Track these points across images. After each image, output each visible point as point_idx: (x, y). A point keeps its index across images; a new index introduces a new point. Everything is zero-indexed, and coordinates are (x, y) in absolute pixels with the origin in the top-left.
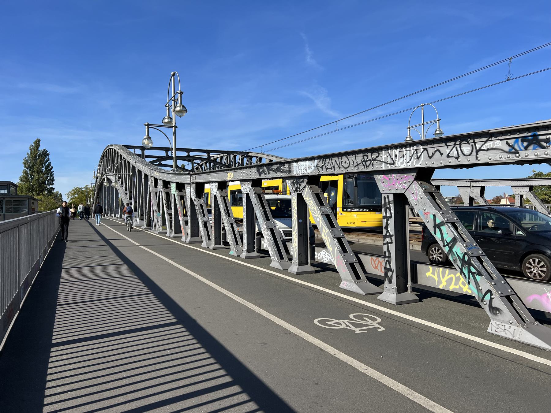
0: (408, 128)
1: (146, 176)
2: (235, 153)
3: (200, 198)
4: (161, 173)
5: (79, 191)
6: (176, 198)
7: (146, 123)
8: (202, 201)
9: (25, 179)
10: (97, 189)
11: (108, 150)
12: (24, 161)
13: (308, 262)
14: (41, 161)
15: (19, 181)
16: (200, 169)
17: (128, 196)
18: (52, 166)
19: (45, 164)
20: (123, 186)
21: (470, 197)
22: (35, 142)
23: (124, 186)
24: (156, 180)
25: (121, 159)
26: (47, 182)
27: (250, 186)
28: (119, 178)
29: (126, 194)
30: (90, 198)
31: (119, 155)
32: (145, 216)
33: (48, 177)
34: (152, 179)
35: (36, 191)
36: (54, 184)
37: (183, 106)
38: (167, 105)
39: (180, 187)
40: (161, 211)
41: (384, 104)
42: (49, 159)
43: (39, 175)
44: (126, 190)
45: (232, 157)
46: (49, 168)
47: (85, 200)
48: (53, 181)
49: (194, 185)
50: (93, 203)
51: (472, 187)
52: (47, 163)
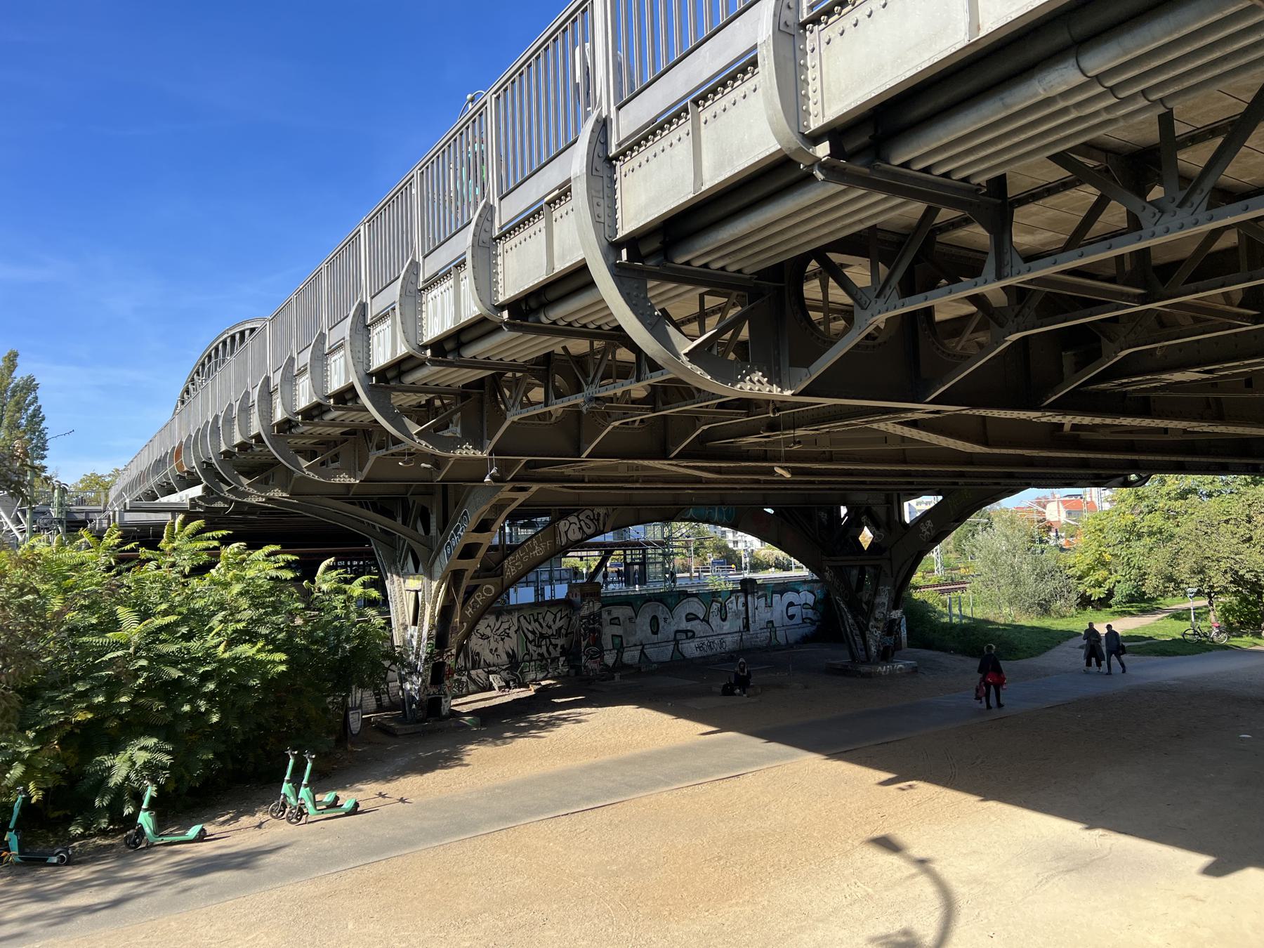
14: (18, 403)
19: (27, 410)
21: (473, 531)
42: (36, 398)
46: (37, 420)
52: (32, 408)
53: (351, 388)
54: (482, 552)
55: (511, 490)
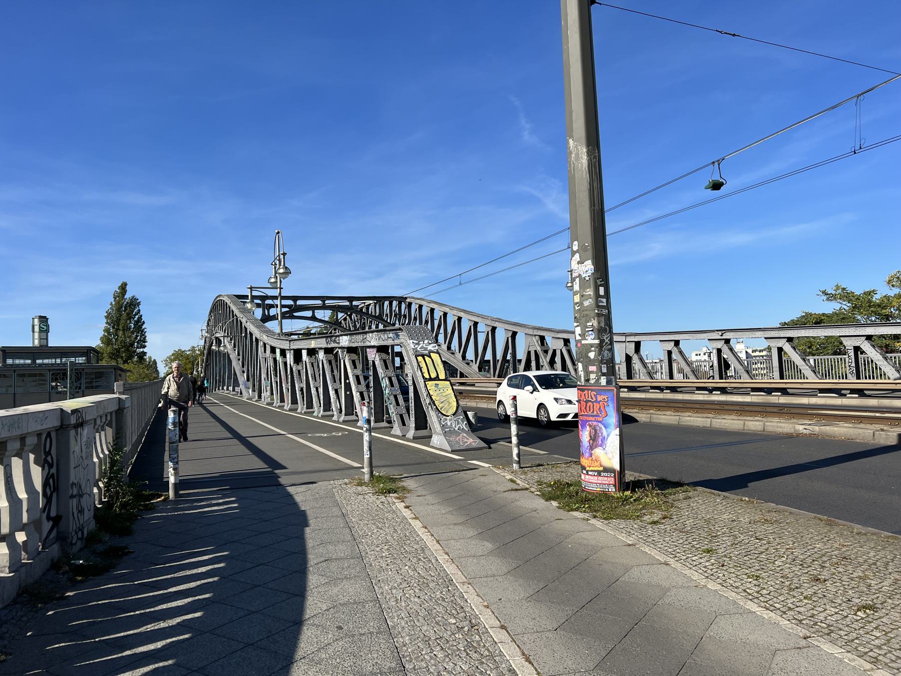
0: (569, 271)
1: (257, 340)
2: (391, 299)
3: (298, 364)
4: (269, 338)
5: (182, 356)
6: (308, 365)
7: (250, 286)
8: (300, 367)
9: (106, 340)
10: (205, 352)
11: (219, 300)
12: (106, 314)
13: (384, 420)
14: (128, 314)
15: (99, 342)
16: (349, 320)
17: (240, 363)
18: (144, 321)
19: (134, 318)
20: (235, 350)
21: (626, 354)
22: (120, 286)
23: (237, 350)
24: (265, 344)
25: (233, 317)
26: (136, 344)
27: (323, 353)
28: (231, 340)
29: (239, 360)
30: (198, 364)
31: (231, 309)
32: (257, 387)
33: (138, 336)
34: (262, 343)
35: (122, 358)
36: (146, 346)
37: (286, 268)
38: (273, 264)
39: (283, 353)
40: (269, 380)
41: (490, 262)
43: (124, 334)
44: (239, 355)
45: (387, 303)
47: (190, 368)
48: (145, 342)
49: (292, 351)
50: (201, 373)
51: (628, 342)
52: (137, 317)
53: (490, 361)
54: (549, 476)
55: (536, 351)
